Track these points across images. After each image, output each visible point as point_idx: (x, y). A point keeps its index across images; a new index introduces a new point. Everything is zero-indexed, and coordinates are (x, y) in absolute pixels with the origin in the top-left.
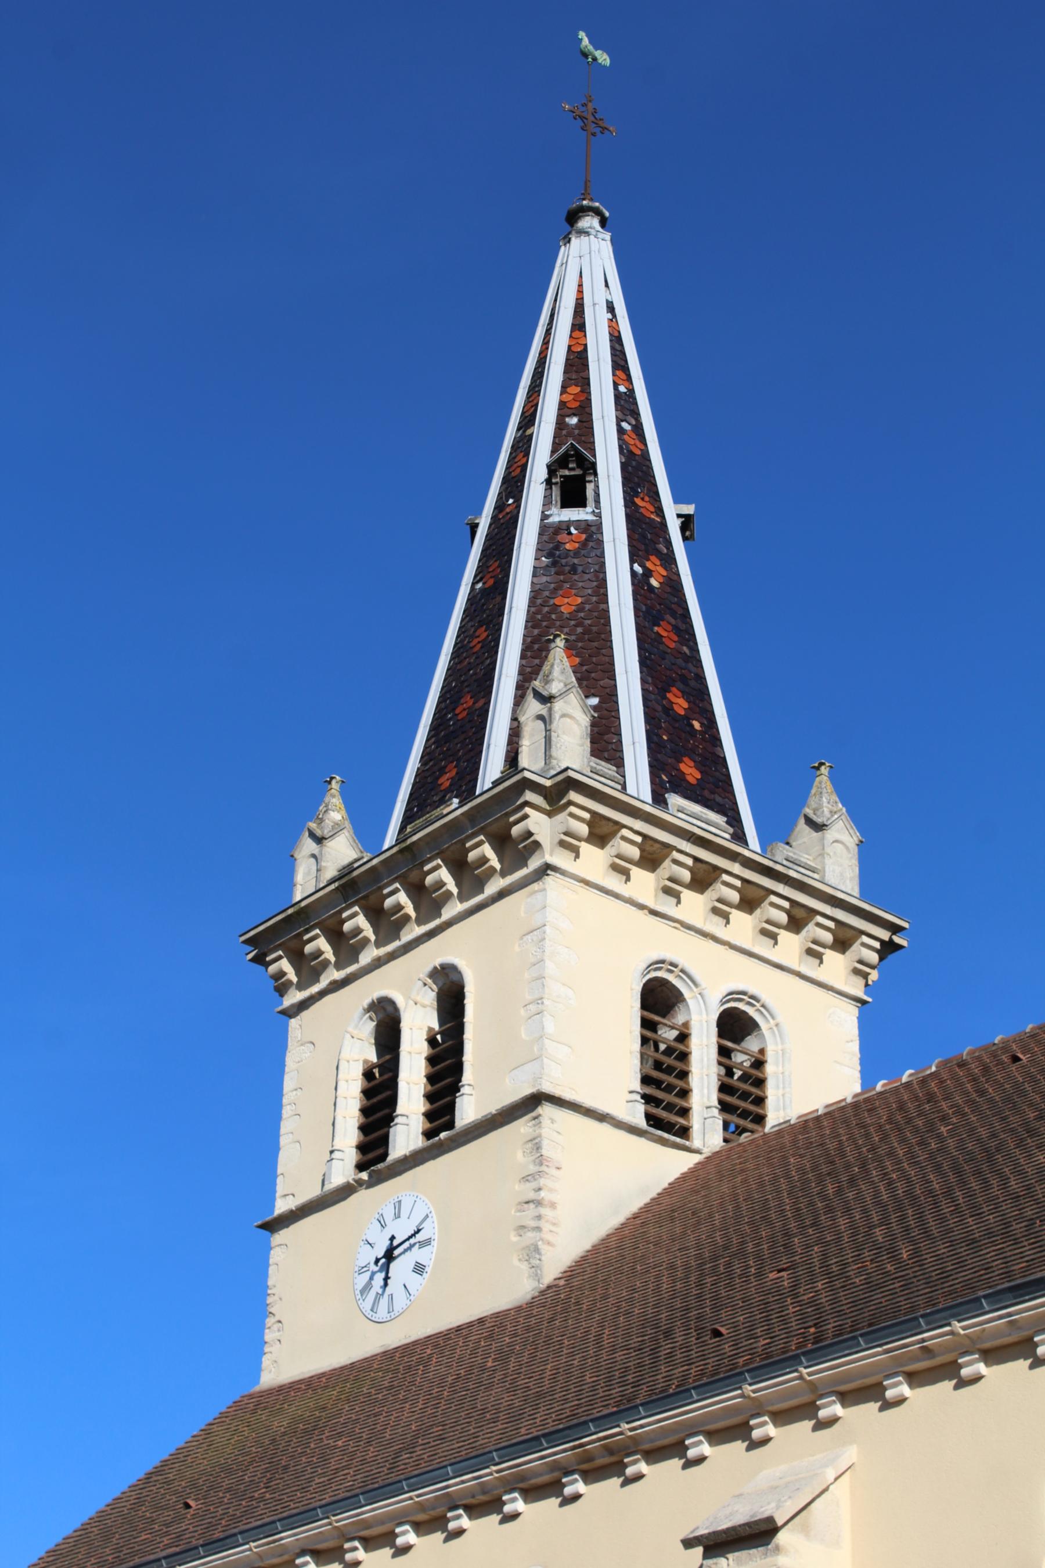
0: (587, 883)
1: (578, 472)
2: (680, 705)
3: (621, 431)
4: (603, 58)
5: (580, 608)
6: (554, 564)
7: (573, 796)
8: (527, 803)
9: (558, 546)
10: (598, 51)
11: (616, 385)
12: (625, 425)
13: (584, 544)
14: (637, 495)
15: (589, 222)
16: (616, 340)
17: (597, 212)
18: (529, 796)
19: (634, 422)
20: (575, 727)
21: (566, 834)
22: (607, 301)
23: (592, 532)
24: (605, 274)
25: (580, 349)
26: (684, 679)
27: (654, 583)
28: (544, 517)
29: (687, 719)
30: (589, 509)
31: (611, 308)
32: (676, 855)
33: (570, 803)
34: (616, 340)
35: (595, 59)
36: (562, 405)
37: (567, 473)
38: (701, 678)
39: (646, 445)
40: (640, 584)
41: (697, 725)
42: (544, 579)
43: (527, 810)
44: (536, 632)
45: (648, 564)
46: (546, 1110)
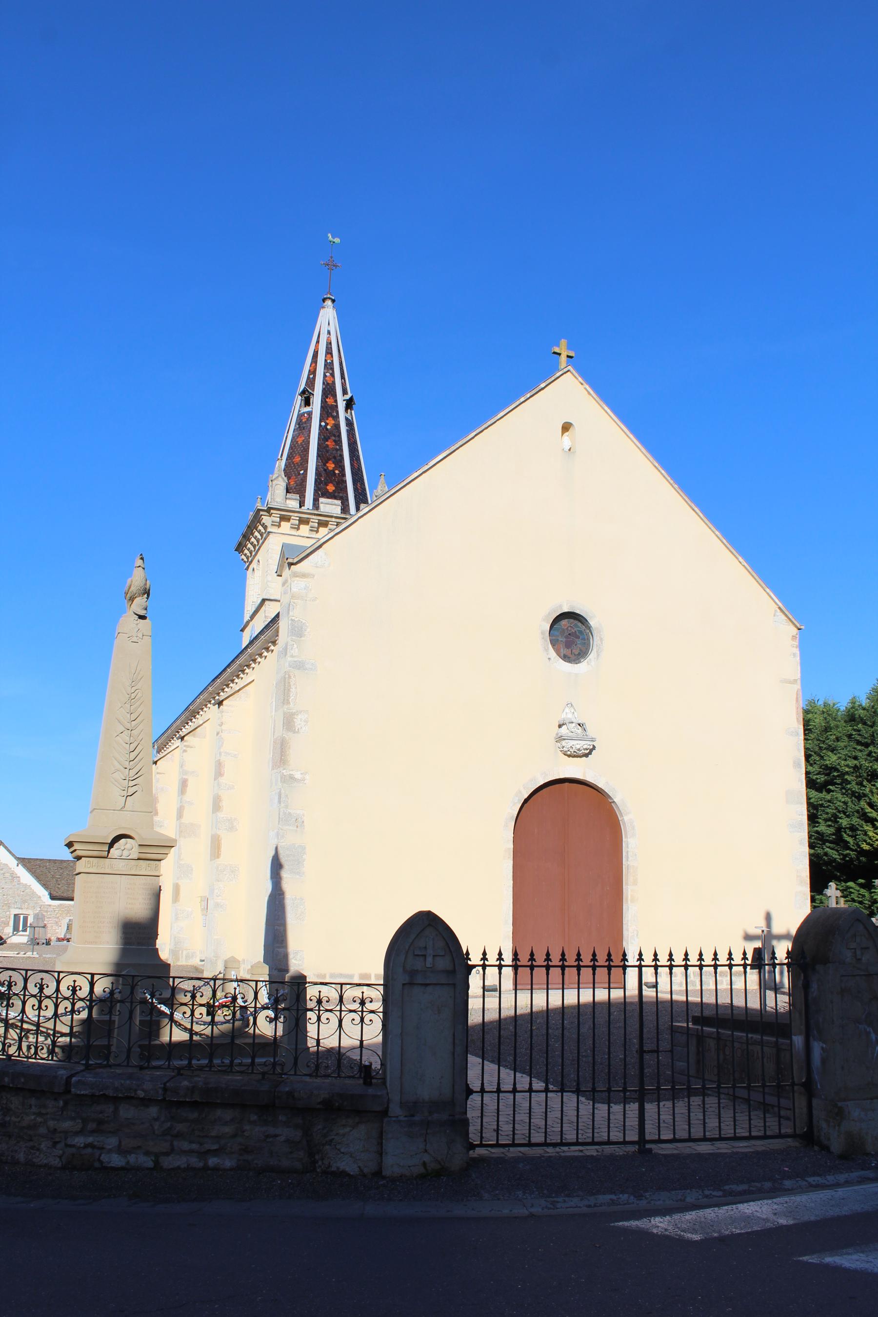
0: (283, 534)
1: (309, 395)
2: (331, 466)
3: (325, 376)
4: (337, 240)
5: (303, 441)
6: (299, 427)
7: (272, 511)
8: (262, 515)
9: (301, 420)
10: (336, 239)
11: (326, 360)
12: (328, 374)
13: (307, 419)
14: (327, 397)
15: (329, 302)
16: (329, 344)
17: (330, 298)
18: (262, 513)
19: (331, 372)
20: (281, 487)
21: (272, 522)
22: (328, 331)
23: (310, 414)
24: (321, 327)
25: (329, 342)
26: (335, 457)
27: (329, 427)
28: (299, 411)
29: (333, 471)
30: (311, 407)
31: (329, 333)
32: (292, 517)
33: (272, 513)
34: (329, 344)
35: (334, 242)
36: (309, 371)
37: (306, 396)
38: (342, 456)
39: (334, 379)
40: (322, 430)
41: (337, 472)
42: (296, 433)
43: (263, 517)
44: (291, 451)
45: (327, 421)
46: (267, 603)
